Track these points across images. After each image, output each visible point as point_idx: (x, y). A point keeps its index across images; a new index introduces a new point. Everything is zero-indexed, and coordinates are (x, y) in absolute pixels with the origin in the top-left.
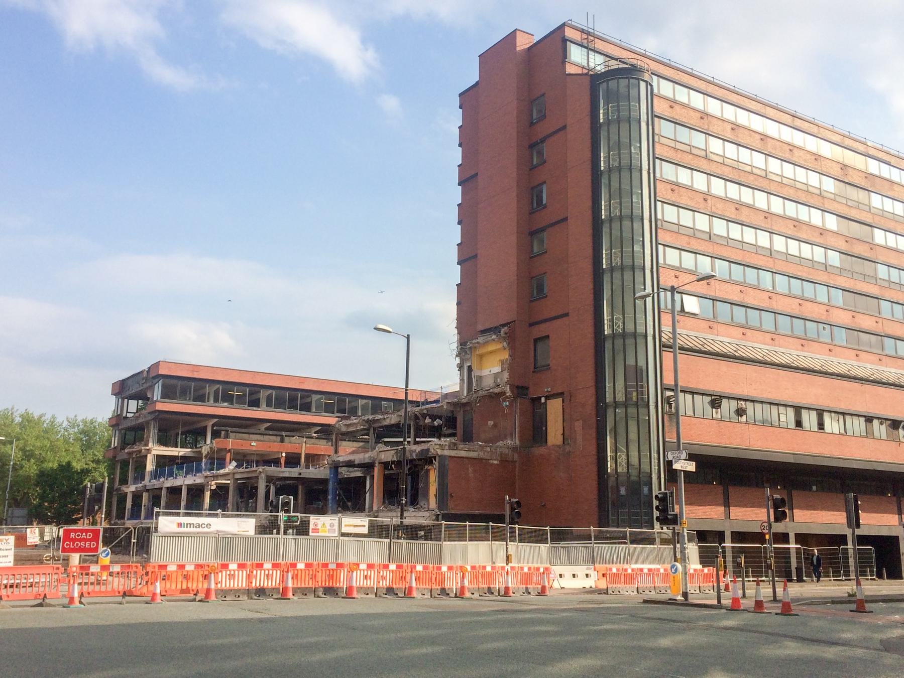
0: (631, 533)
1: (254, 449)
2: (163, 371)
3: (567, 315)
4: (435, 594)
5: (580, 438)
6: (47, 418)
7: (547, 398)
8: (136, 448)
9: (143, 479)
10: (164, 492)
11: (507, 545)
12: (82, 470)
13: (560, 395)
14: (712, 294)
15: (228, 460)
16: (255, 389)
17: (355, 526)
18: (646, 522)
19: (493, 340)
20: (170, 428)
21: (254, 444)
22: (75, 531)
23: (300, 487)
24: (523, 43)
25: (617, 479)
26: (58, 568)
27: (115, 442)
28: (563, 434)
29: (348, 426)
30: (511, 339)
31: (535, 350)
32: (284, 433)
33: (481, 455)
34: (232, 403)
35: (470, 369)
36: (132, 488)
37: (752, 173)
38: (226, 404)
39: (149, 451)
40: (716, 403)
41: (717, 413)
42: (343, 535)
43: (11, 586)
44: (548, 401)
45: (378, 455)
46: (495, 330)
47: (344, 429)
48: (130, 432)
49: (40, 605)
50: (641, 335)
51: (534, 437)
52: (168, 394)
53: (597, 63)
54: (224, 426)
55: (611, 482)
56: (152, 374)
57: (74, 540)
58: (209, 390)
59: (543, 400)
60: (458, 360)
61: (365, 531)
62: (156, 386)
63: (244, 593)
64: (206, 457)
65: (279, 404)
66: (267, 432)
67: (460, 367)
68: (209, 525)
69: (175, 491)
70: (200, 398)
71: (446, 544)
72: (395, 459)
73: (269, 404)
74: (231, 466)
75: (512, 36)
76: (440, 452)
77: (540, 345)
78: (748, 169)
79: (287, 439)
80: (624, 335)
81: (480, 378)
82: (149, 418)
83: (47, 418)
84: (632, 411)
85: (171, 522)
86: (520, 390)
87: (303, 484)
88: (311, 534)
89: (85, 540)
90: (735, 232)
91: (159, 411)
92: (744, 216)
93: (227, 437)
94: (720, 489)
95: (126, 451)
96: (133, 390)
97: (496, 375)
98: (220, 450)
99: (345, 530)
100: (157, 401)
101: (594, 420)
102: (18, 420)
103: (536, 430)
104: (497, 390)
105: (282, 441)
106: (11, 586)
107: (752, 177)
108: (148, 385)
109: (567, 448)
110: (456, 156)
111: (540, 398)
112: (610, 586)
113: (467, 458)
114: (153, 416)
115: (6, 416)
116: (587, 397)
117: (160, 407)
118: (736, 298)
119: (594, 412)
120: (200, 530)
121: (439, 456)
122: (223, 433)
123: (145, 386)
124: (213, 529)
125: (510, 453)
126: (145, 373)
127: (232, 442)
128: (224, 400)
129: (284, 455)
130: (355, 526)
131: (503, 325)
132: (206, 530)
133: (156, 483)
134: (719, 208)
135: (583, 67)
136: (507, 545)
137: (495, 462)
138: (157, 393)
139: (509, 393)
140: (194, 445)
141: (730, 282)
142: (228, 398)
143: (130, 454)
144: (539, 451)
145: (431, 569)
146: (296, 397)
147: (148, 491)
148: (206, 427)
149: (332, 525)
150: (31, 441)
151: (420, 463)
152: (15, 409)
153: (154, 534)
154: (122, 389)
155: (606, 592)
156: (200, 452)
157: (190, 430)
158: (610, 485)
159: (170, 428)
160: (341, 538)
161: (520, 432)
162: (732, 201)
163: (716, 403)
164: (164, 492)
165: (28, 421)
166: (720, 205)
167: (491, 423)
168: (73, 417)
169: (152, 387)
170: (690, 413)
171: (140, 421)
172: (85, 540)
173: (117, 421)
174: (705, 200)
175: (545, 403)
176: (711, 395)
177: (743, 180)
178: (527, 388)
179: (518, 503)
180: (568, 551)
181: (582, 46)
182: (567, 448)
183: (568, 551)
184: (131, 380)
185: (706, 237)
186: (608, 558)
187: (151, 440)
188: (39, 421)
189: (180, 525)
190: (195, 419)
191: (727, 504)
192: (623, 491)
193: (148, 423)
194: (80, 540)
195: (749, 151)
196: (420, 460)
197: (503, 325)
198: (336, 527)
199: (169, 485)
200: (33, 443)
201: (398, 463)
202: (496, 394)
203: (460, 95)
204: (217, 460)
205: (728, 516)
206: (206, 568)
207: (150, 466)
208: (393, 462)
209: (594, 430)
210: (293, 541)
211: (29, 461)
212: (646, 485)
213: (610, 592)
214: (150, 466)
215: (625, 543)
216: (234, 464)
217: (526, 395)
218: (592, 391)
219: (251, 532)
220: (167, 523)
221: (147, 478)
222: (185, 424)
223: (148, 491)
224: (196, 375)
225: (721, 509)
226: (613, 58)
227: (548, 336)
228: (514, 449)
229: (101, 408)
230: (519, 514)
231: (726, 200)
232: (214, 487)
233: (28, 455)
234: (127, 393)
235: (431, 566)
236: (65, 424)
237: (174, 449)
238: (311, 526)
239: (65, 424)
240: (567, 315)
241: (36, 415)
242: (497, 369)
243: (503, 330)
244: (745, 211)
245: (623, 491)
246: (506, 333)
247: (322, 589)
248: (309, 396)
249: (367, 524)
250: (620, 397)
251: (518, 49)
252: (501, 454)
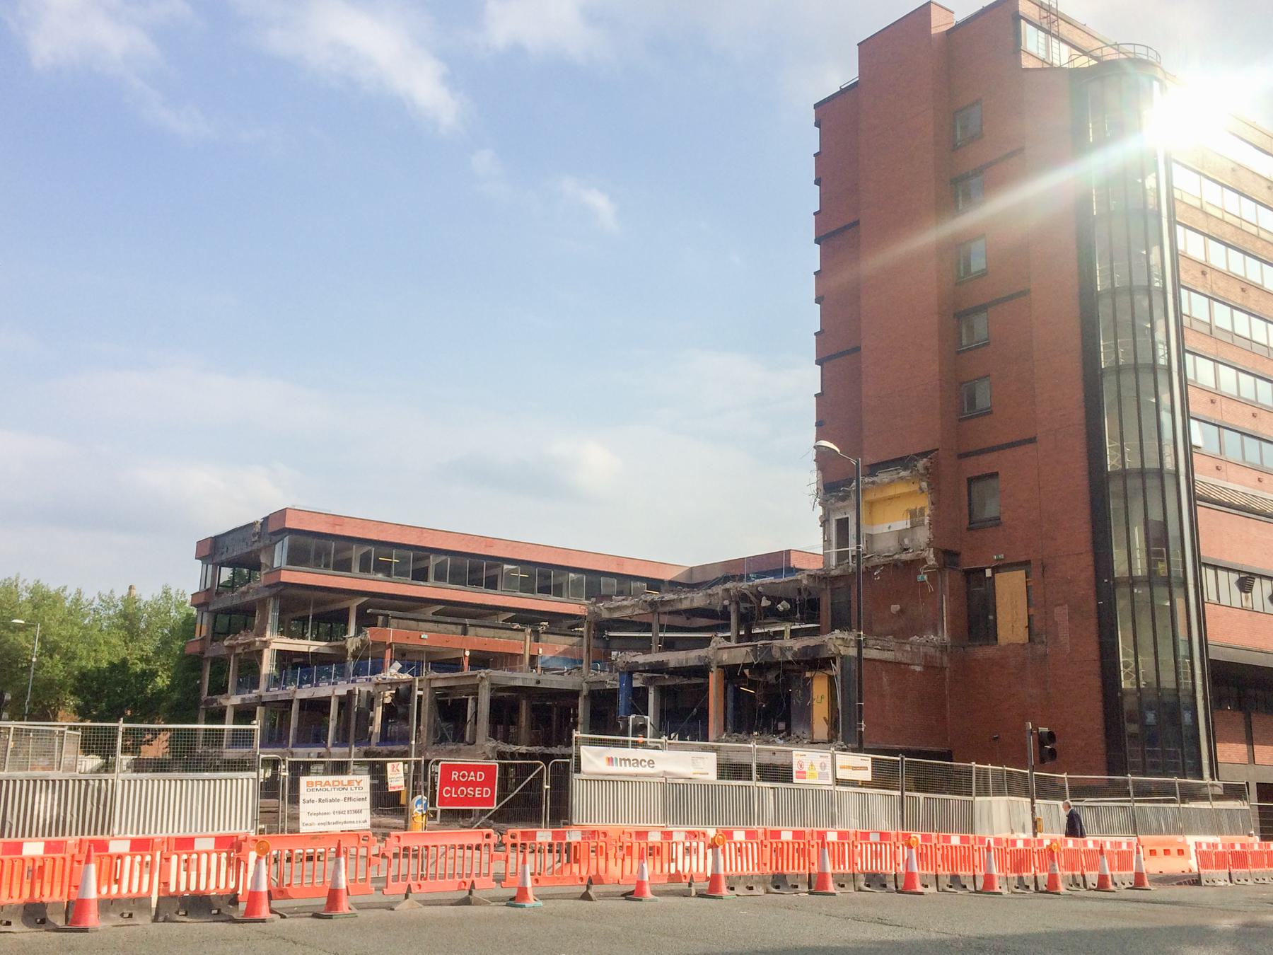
0: (1180, 784)
1: (425, 643)
2: (289, 524)
3: (1032, 440)
4: (943, 885)
5: (1064, 636)
6: (71, 592)
7: (995, 570)
8: (241, 639)
9: (257, 687)
10: (295, 707)
11: (1033, 802)
12: (143, 672)
13: (1024, 564)
14: (1217, 418)
15: (388, 658)
16: (423, 552)
17: (855, 768)
18: (1191, 769)
19: (901, 478)
20: (304, 610)
21: (426, 637)
22: (459, 768)
23: (524, 702)
24: (939, 24)
25: (1140, 699)
26: (488, 836)
27: (203, 630)
28: (1029, 627)
29: (609, 609)
30: (934, 478)
31: (969, 494)
32: (467, 621)
33: (900, 657)
34: (389, 575)
35: (843, 525)
36: (236, 700)
37: (1258, 237)
38: (380, 576)
39: (266, 644)
40: (1245, 583)
41: (1247, 599)
42: (840, 782)
43: (310, 858)
44: (997, 576)
45: (715, 653)
46: (903, 462)
47: (605, 615)
48: (227, 613)
49: (466, 902)
50: (1151, 471)
51: (970, 632)
52: (297, 557)
53: (1061, 56)
54: (374, 610)
55: (1129, 704)
56: (272, 528)
57: (457, 784)
58: (356, 553)
59: (988, 573)
60: (819, 511)
61: (867, 776)
62: (278, 546)
63: (758, 883)
64: (354, 656)
65: (457, 577)
66: (435, 618)
67: (825, 522)
68: (651, 762)
69: (316, 708)
70: (343, 566)
71: (978, 799)
72: (750, 659)
73: (440, 577)
74: (393, 672)
75: (923, 13)
76: (843, 651)
77: (976, 488)
78: (1253, 230)
79: (471, 631)
80: (1142, 473)
81: (871, 538)
82: (267, 594)
83: (71, 592)
84: (1160, 592)
85: (599, 755)
86: (948, 557)
87: (529, 698)
88: (795, 780)
89: (474, 784)
90: (1242, 324)
91: (286, 584)
92: (1253, 300)
93: (386, 624)
94: (1239, 716)
95: (226, 643)
96: (237, 551)
97: (901, 534)
98: (375, 644)
99: (841, 774)
100: (279, 569)
101: (1093, 605)
102: (25, 596)
103: (978, 620)
104: (905, 557)
105: (465, 633)
106: (310, 858)
107: (1259, 244)
108: (262, 544)
109: (1040, 649)
110: (812, 198)
111: (983, 570)
112: (1202, 871)
113: (880, 661)
114: (274, 590)
115: (9, 589)
116: (1080, 568)
117: (288, 576)
118: (1248, 426)
119: (1091, 592)
120: (639, 770)
121: (842, 657)
122: (380, 618)
123: (256, 546)
124: (659, 768)
125: (938, 654)
126: (258, 526)
127: (393, 634)
128: (377, 570)
129: (467, 653)
130: (855, 768)
131: (924, 455)
132: (648, 770)
133: (280, 693)
134: (1221, 287)
135: (1043, 61)
136: (1033, 802)
137: (918, 669)
138: (280, 555)
139: (932, 560)
140: (329, 636)
141: (1237, 400)
142: (385, 568)
143: (231, 647)
144: (982, 652)
145: (934, 841)
146: (478, 567)
147: (264, 704)
148: (347, 610)
149: (823, 766)
150: (55, 627)
151: (796, 667)
152: (21, 580)
153: (576, 776)
154: (212, 551)
155: (1196, 881)
156: (344, 649)
157: (321, 613)
158: (1126, 707)
159: (304, 610)
160: (837, 788)
161: (951, 622)
162: (1235, 278)
163: (1245, 583)
164: (295, 707)
165: (42, 600)
166: (1222, 283)
167: (895, 608)
168: (108, 593)
169: (270, 549)
170: (1213, 598)
171: (248, 598)
172: (474, 784)
173: (203, 601)
174: (1204, 273)
175: (993, 578)
176: (1239, 572)
177: (1248, 247)
178: (957, 554)
179: (1051, 736)
180: (1097, 815)
181: (1039, 28)
182: (1040, 649)
183: (1097, 815)
184: (231, 536)
185: (1206, 330)
186: (1154, 825)
187: (269, 627)
188: (56, 599)
189: (610, 760)
190: (332, 596)
191: (1250, 742)
192: (1151, 717)
193: (263, 603)
194: (467, 784)
195: (1254, 204)
196: (798, 662)
197: (924, 455)
198: (829, 770)
199: (304, 696)
200: (58, 632)
201: (759, 668)
202: (905, 563)
203: (816, 106)
204: (369, 661)
205: (1252, 760)
206: (602, 837)
207: (268, 666)
208: (746, 666)
209: (1094, 621)
210: (771, 792)
211: (51, 657)
212: (1187, 709)
213: (1204, 882)
214: (268, 666)
215: (1173, 801)
216: (398, 665)
217: (957, 565)
218: (1088, 560)
219: (712, 776)
220: (595, 759)
221: (263, 684)
222: (318, 603)
223: (264, 704)
224: (338, 531)
225: (1243, 748)
226: (1085, 53)
227: (997, 474)
228: (943, 649)
229: (187, 579)
230: (1053, 753)
231: (1227, 275)
232: (388, 700)
233: (50, 649)
234: (224, 558)
235: (934, 835)
236: (96, 603)
237: (301, 641)
238: (795, 768)
239: (96, 603)
240: (1032, 440)
241: (53, 587)
242: (903, 524)
243: (921, 463)
244: (1253, 293)
245: (1151, 717)
246: (926, 468)
247: (862, 877)
248: (497, 566)
249: (869, 764)
250: (1140, 568)
251: (933, 31)
252: (926, 654)
